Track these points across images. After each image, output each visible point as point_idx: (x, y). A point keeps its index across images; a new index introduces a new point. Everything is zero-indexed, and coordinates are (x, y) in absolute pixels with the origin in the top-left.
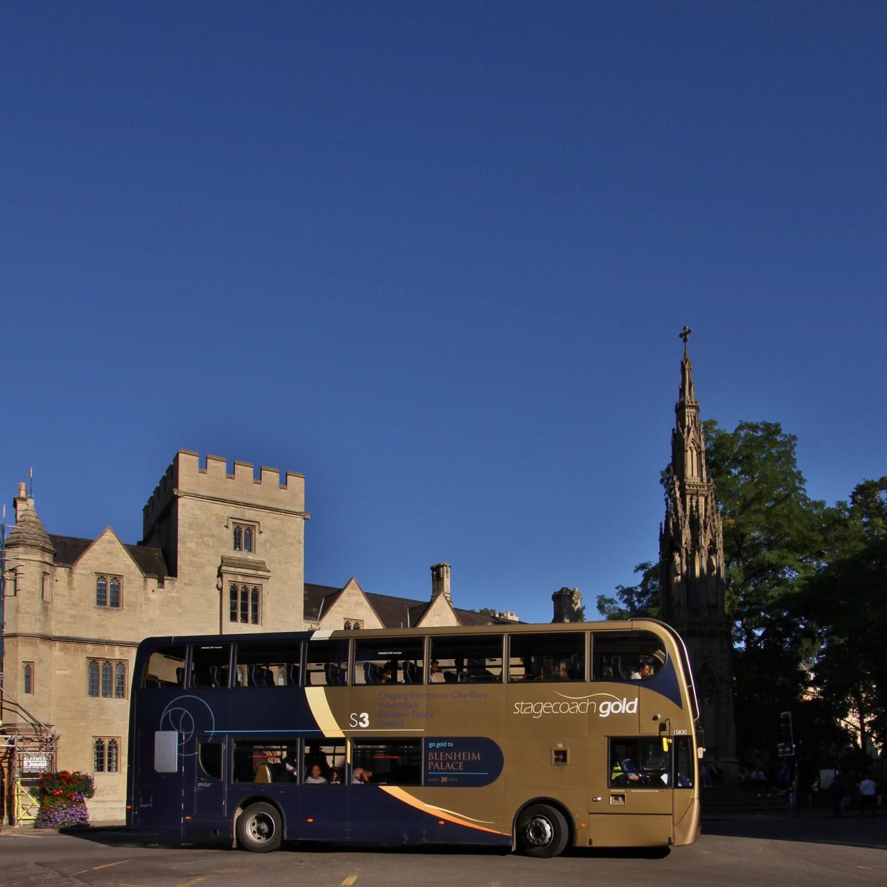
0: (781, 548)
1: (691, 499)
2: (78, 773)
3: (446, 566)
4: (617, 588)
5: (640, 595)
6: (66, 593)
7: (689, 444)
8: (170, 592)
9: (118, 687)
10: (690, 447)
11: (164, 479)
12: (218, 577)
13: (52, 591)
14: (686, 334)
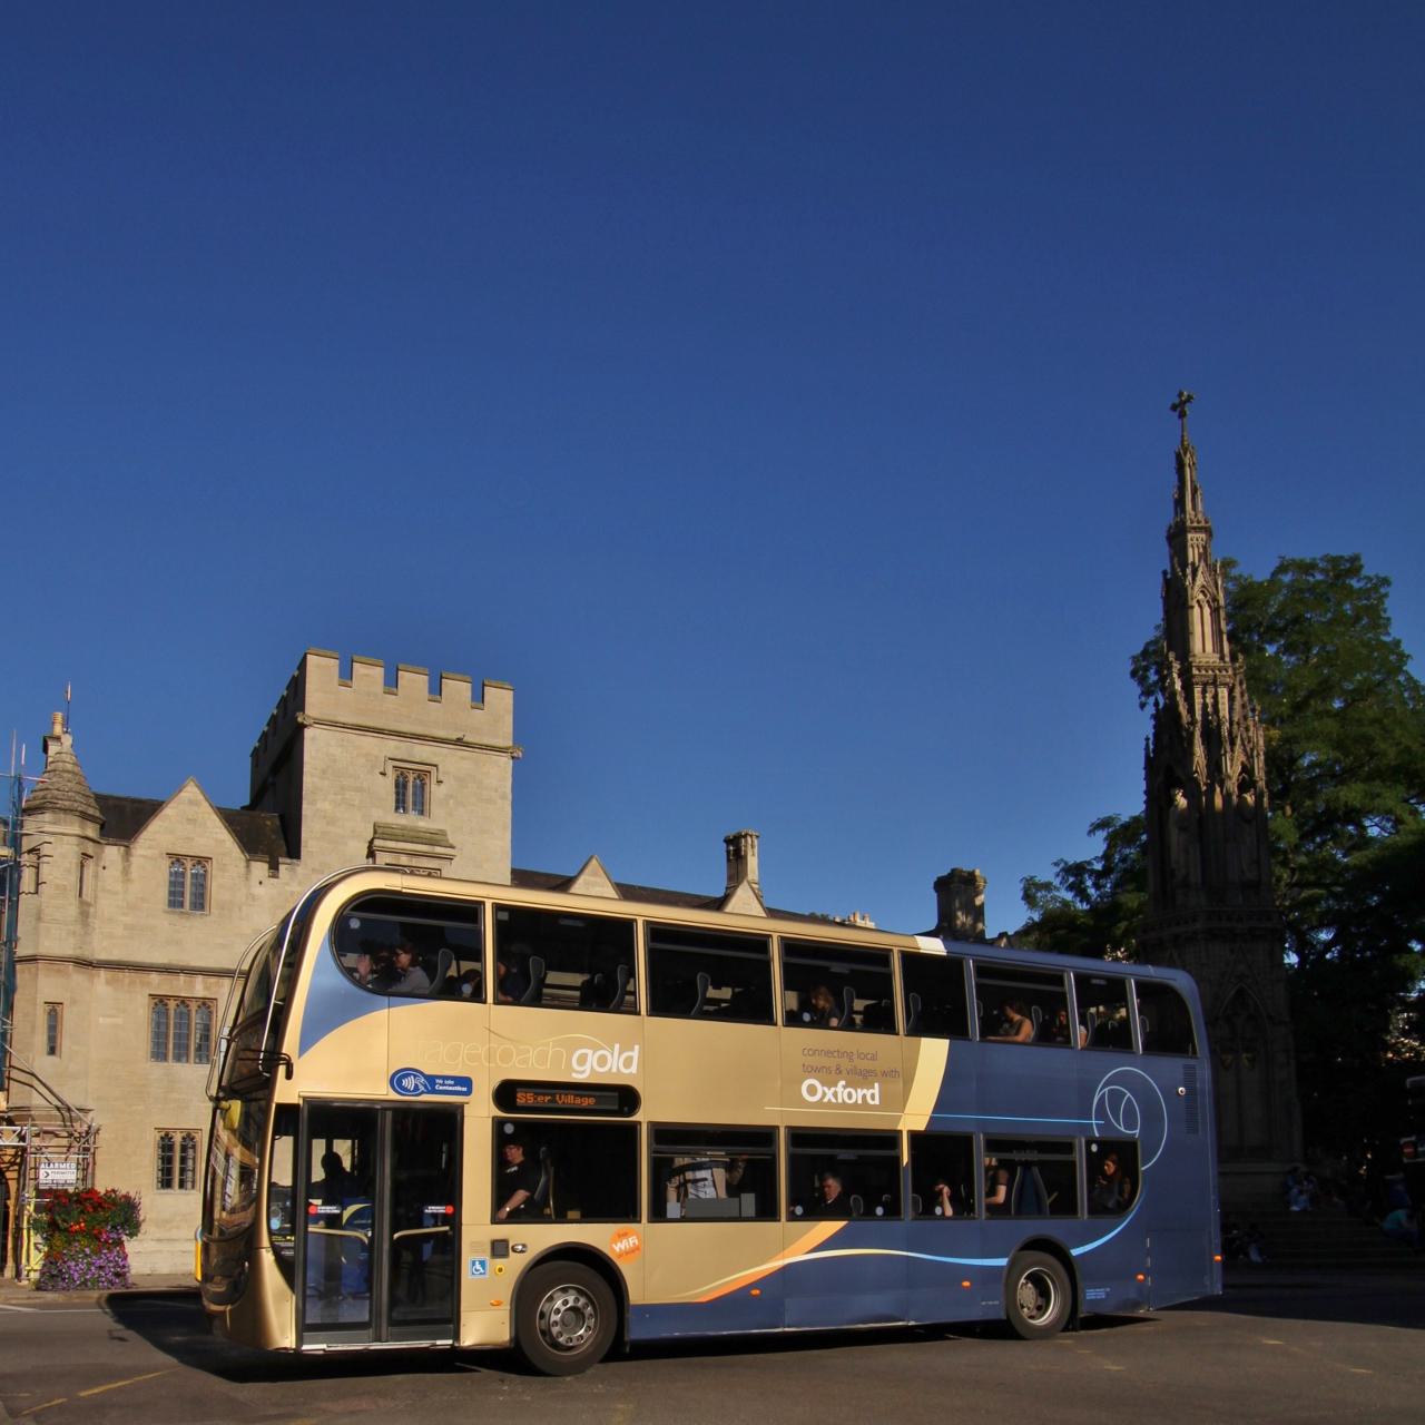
0: (1369, 778)
1: (1204, 692)
2: (114, 1191)
3: (751, 836)
4: (1056, 864)
5: (1099, 875)
6: (119, 887)
7: (1196, 594)
8: (287, 884)
9: (200, 1046)
10: (1198, 601)
11: (284, 700)
12: (367, 857)
13: (96, 886)
14: (1183, 403)
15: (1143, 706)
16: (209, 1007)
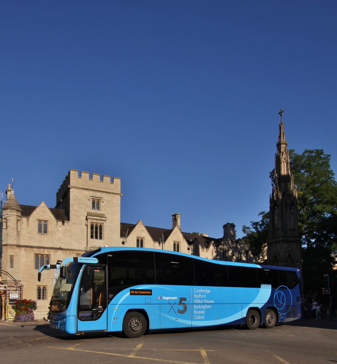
0: (323, 204)
2: (31, 300)
4: (251, 222)
5: (261, 225)
7: (283, 160)
8: (67, 227)
10: (283, 161)
13: (21, 227)
15: (188, 249)
16: (48, 257)
